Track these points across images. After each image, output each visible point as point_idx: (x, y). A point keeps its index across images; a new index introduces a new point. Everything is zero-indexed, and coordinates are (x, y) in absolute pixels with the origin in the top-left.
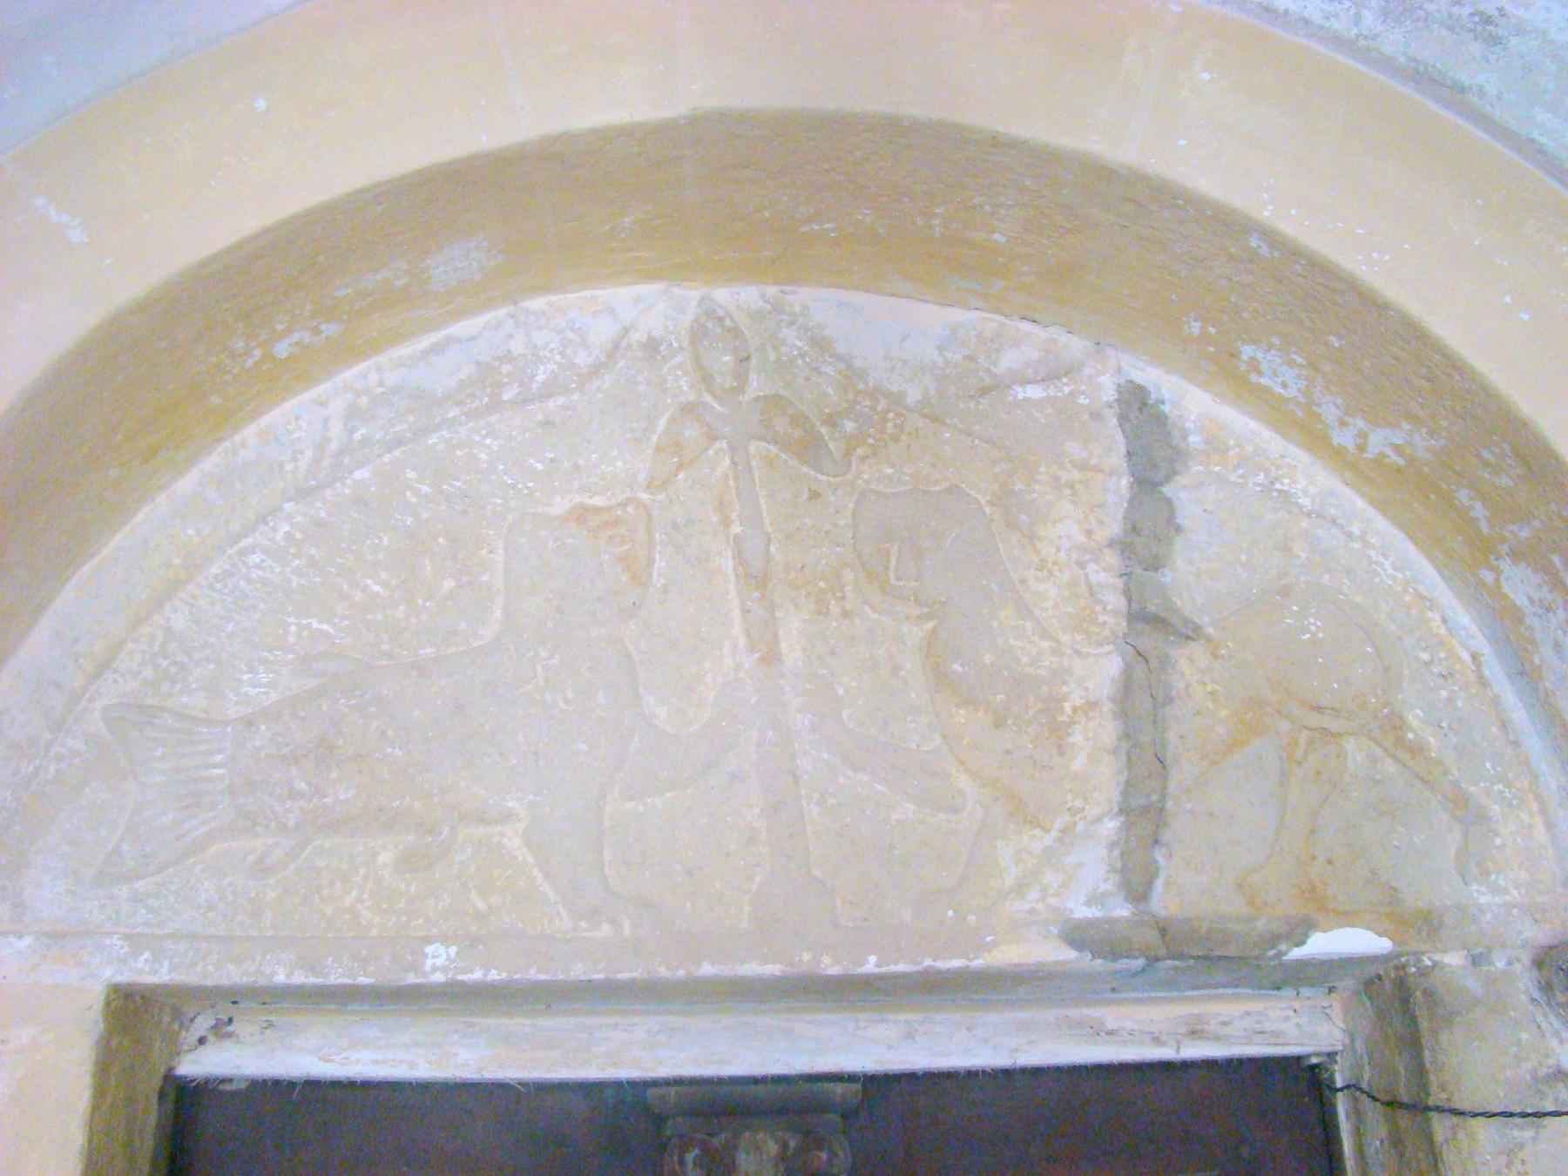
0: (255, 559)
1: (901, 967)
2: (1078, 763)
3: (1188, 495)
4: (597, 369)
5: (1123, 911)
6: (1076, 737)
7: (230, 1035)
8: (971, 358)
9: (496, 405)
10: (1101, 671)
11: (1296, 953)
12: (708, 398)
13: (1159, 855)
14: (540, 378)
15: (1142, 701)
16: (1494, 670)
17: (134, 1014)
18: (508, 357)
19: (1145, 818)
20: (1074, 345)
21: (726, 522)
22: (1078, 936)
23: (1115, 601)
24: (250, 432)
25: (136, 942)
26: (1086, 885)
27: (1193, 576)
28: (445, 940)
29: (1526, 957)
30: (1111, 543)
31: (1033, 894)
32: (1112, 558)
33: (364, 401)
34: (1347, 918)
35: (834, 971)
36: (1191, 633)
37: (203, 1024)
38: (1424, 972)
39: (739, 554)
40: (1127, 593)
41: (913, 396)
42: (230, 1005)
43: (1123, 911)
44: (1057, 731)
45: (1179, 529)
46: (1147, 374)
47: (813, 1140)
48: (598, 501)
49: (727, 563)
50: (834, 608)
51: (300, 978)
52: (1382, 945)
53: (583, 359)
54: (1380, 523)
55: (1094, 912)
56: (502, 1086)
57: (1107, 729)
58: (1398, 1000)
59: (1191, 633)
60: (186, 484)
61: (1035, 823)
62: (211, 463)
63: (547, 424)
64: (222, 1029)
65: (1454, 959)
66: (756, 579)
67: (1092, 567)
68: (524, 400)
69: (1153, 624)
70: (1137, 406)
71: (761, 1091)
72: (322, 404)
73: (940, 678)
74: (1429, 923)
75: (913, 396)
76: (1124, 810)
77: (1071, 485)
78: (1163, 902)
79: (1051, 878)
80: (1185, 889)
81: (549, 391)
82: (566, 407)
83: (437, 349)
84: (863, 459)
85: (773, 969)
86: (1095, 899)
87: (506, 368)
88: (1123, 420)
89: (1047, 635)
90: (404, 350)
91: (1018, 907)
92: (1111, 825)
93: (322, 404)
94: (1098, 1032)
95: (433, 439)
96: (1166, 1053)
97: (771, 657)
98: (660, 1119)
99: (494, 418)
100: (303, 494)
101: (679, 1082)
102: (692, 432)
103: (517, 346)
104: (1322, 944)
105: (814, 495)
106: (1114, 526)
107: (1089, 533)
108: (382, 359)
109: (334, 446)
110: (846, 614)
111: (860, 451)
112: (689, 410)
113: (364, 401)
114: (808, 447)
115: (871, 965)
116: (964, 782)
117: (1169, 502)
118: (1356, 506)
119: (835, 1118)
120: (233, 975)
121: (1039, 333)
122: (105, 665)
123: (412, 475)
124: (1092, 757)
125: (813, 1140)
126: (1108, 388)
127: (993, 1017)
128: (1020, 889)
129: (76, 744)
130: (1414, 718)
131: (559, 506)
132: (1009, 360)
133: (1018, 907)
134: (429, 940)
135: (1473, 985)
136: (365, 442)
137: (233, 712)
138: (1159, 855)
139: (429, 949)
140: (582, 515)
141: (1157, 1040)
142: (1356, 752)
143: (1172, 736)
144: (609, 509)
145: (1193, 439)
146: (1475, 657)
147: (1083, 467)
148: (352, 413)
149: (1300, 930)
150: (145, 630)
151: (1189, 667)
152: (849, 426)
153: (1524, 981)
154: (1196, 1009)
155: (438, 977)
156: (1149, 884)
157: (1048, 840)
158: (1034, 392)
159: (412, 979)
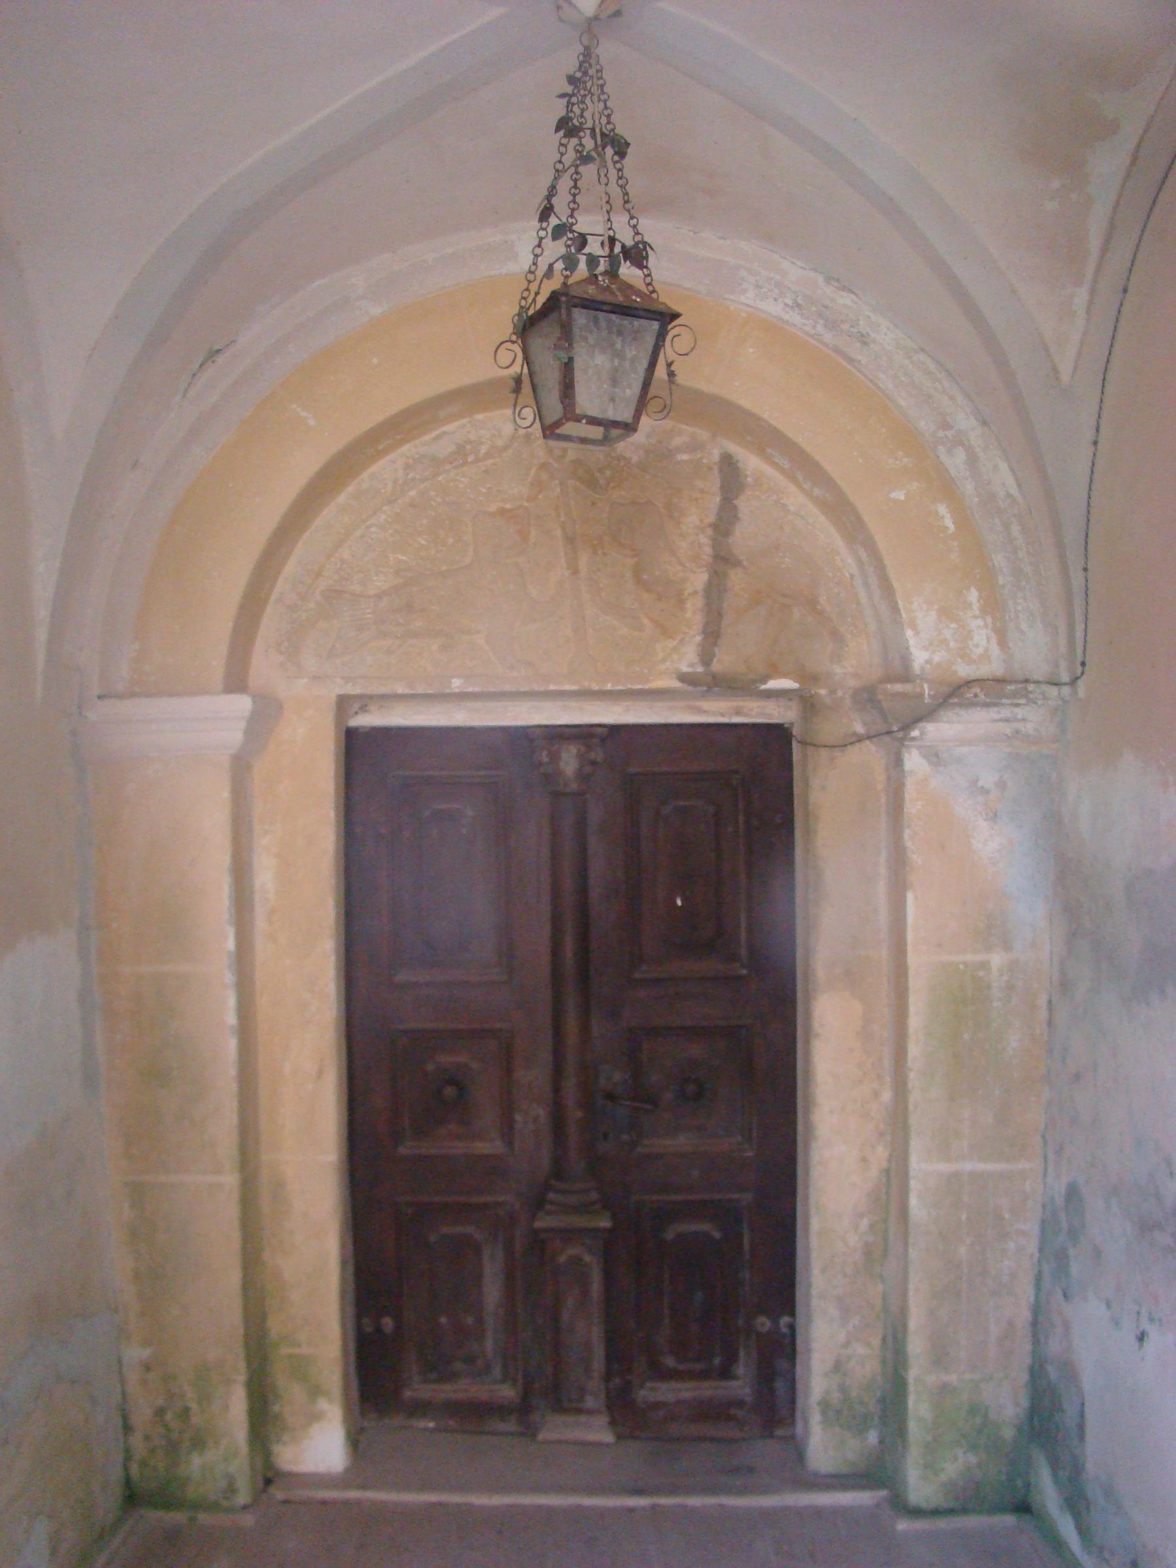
0: (374, 529)
1: (620, 688)
2: (689, 615)
3: (745, 504)
4: (506, 447)
5: (700, 669)
6: (688, 605)
7: (367, 711)
8: (660, 442)
9: (465, 463)
10: (700, 579)
11: (763, 687)
12: (551, 461)
13: (716, 650)
14: (483, 452)
15: (715, 590)
16: (858, 581)
17: (343, 704)
18: (470, 442)
19: (712, 635)
20: (703, 435)
21: (559, 516)
22: (683, 678)
23: (708, 550)
24: (365, 475)
25: (347, 679)
26: (688, 660)
27: (743, 538)
28: (459, 677)
29: (851, 691)
30: (711, 525)
31: (668, 663)
32: (709, 531)
33: (411, 461)
34: (785, 675)
35: (596, 688)
36: (737, 563)
37: (356, 707)
38: (811, 697)
39: (564, 529)
40: (713, 547)
41: (635, 459)
42: (364, 702)
43: (700, 669)
44: (681, 602)
45: (738, 519)
46: (734, 449)
47: (589, 748)
48: (508, 506)
49: (558, 533)
50: (600, 552)
51: (408, 691)
52: (796, 686)
53: (500, 443)
54: (822, 518)
55: (690, 670)
56: (471, 729)
57: (699, 602)
58: (809, 705)
59: (737, 563)
60: (342, 498)
61: (671, 637)
62: (351, 489)
63: (486, 472)
64: (364, 709)
65: (823, 692)
66: (570, 540)
67: (701, 536)
68: (477, 460)
69: (723, 561)
70: (728, 464)
71: (567, 730)
72: (394, 462)
73: (638, 581)
74: (814, 679)
75: (635, 459)
76: (703, 632)
77: (696, 499)
78: (716, 666)
79: (675, 657)
80: (723, 662)
81: (488, 455)
82: (494, 464)
83: (437, 438)
84: (614, 488)
85: (574, 688)
86: (691, 665)
87: (469, 447)
88: (721, 471)
89: (681, 564)
90: (427, 438)
91: (663, 667)
92: (699, 638)
93: (394, 462)
94: (700, 711)
95: (440, 478)
96: (725, 720)
97: (575, 572)
98: (532, 740)
99: (465, 469)
100: (390, 502)
101: (539, 726)
102: (544, 476)
103: (472, 437)
104: (773, 684)
105: (593, 504)
106: (711, 518)
107: (701, 520)
108: (417, 442)
109: (400, 482)
110: (604, 554)
111: (612, 485)
112: (543, 466)
113: (411, 461)
114: (591, 483)
115: (609, 687)
116: (646, 621)
117: (735, 507)
118: (813, 509)
119: (596, 741)
120: (382, 690)
121: (690, 429)
122: (319, 574)
123: (433, 494)
124: (694, 612)
125: (589, 748)
126: (716, 454)
127: (660, 704)
128: (664, 660)
129: (312, 605)
130: (823, 599)
131: (493, 508)
132: (677, 441)
133: (663, 667)
134: (453, 677)
135: (828, 701)
136: (413, 479)
137: (372, 592)
138: (716, 650)
139: (454, 680)
140: (502, 512)
141: (722, 715)
142: (796, 613)
143: (725, 605)
144: (512, 510)
145: (749, 479)
146: (852, 576)
147: (702, 491)
148: (407, 467)
149: (765, 679)
150: (333, 559)
151: (736, 578)
152: (608, 473)
153: (848, 701)
154: (741, 704)
155: (457, 690)
156: (711, 660)
157: (675, 643)
158: (685, 457)
159: (448, 691)
